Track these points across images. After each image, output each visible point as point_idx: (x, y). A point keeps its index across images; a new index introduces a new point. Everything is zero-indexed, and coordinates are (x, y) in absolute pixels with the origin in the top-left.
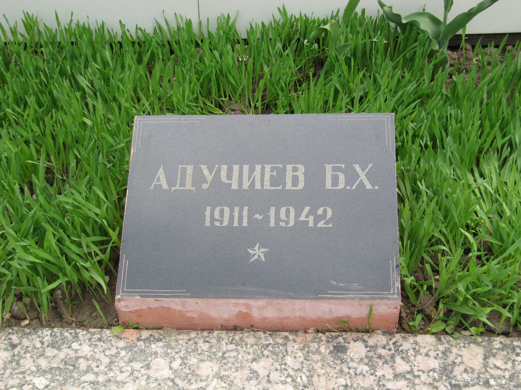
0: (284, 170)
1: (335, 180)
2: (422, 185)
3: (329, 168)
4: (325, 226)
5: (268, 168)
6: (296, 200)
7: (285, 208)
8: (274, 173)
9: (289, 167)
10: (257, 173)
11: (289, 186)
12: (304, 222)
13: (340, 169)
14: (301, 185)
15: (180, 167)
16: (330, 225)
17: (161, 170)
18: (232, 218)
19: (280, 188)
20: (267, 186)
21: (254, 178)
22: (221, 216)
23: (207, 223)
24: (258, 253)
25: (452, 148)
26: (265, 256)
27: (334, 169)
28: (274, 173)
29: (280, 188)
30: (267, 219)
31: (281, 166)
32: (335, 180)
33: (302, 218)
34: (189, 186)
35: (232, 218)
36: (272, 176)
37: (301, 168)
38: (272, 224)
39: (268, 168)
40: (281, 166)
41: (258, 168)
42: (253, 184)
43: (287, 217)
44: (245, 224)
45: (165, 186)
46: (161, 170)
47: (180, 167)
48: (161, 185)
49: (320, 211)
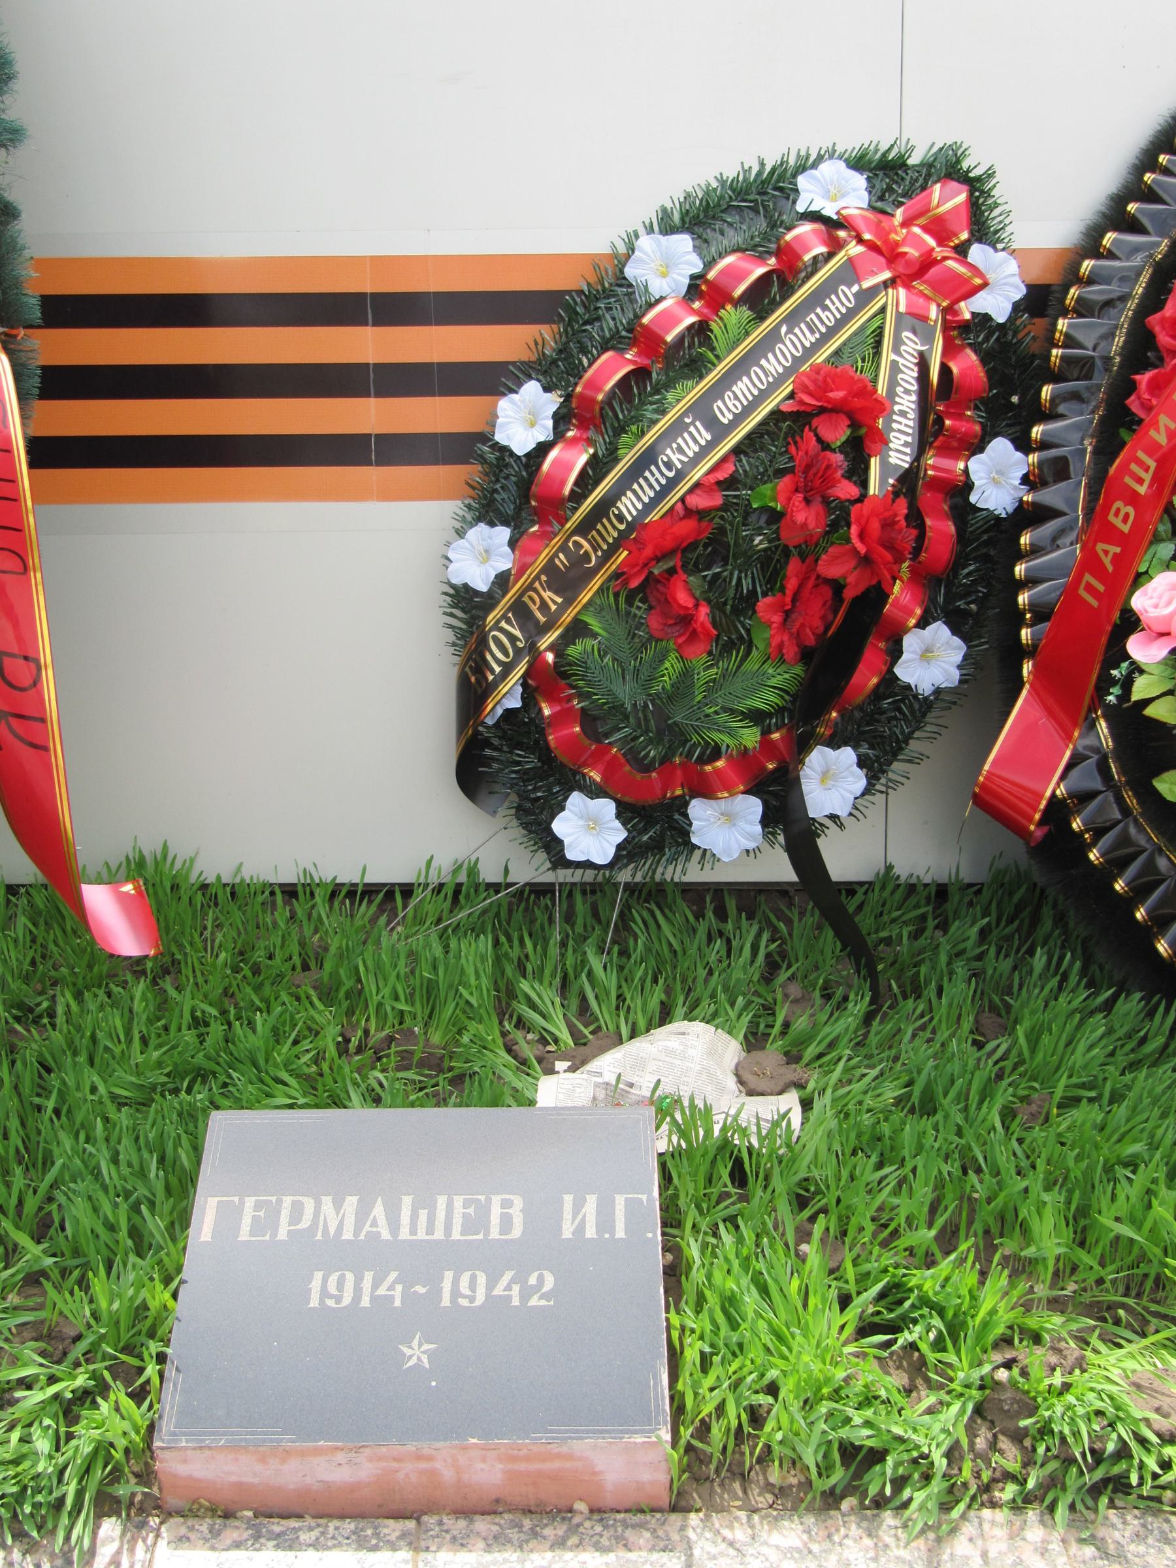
4: (543, 1303)
5: (458, 1201)
6: (492, 1258)
7: (536, 1274)
8: (262, 1214)
9: (496, 1200)
11: (495, 1234)
14: (517, 1232)
17: (379, 1202)
18: (358, 1290)
19: (480, 1236)
20: (456, 1235)
21: (325, 1222)
22: (331, 1289)
23: (314, 1303)
24: (417, 1353)
28: (471, 1210)
29: (480, 1236)
31: (482, 1198)
33: (498, 1291)
34: (495, 1234)
35: (358, 1290)
36: (255, 1219)
37: (518, 1202)
38: (446, 1301)
39: (458, 1201)
40: (482, 1198)
42: (580, 1229)
43: (470, 1289)
44: (365, 1302)
45: (386, 1235)
46: (379, 1202)
48: (379, 1233)
49: (533, 1280)
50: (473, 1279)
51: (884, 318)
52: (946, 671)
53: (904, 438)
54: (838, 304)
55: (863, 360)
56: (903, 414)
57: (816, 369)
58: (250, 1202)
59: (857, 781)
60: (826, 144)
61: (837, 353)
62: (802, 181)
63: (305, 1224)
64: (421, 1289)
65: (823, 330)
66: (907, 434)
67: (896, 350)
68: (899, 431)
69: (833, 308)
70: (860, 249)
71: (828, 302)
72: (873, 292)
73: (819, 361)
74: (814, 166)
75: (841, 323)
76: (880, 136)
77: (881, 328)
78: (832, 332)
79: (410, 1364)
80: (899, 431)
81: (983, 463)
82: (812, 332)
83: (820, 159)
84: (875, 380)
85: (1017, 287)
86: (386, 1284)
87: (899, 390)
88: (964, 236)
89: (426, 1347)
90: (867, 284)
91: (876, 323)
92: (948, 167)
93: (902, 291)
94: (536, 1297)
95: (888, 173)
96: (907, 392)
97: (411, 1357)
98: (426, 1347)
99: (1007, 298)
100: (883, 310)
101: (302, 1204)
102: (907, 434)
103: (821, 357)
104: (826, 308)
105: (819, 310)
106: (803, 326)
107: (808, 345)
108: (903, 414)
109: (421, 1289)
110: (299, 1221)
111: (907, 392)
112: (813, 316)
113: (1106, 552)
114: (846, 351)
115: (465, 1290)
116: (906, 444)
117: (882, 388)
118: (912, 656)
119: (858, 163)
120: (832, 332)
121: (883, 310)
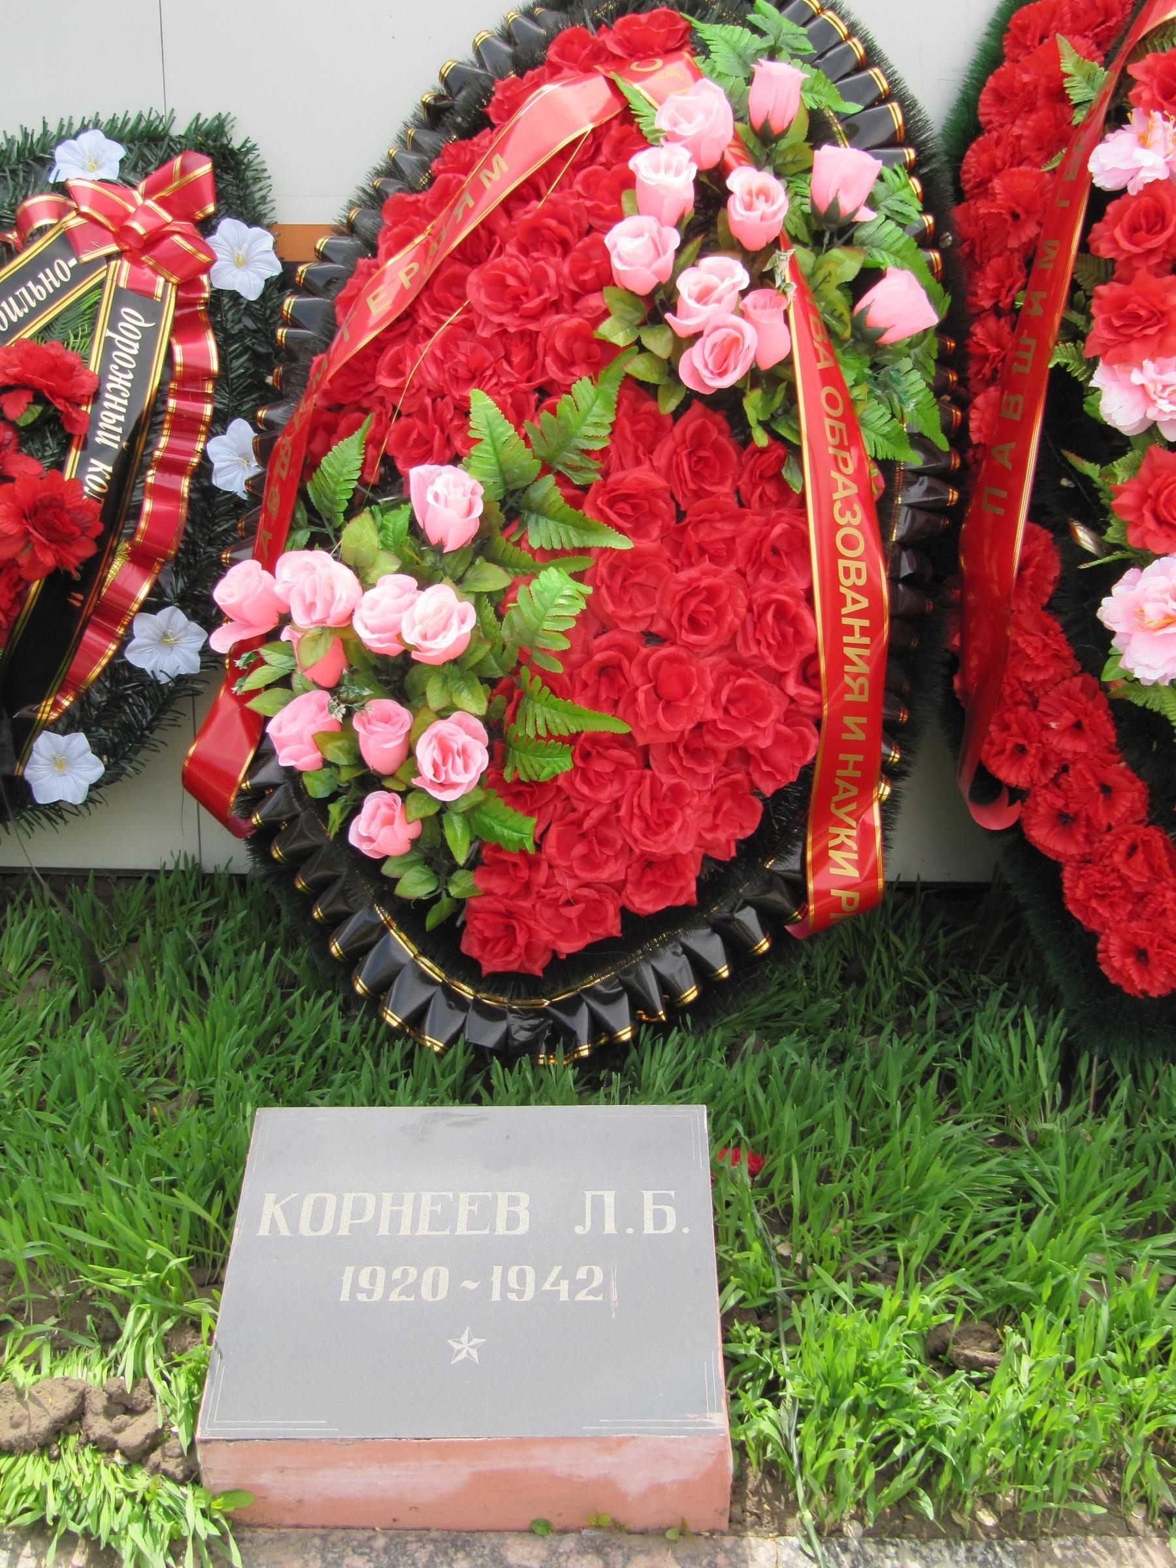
0: (495, 1198)
1: (660, 1219)
2: (273, 1222)
3: (648, 1196)
4: (591, 1298)
8: (438, 1208)
9: (503, 1198)
10: (407, 1210)
11: (501, 1229)
12: (548, 1292)
13: (666, 1200)
14: (523, 1229)
15: (589, 1194)
16: (600, 1298)
20: (423, 1230)
22: (365, 1284)
23: (345, 1297)
24: (466, 1347)
25: (902, 1164)
26: (451, 1349)
27: (657, 1200)
30: (487, 1287)
31: (489, 1194)
32: (660, 1219)
33: (547, 1286)
36: (433, 1214)
37: (525, 1199)
38: (496, 1296)
39: (426, 1198)
41: (409, 1197)
43: (515, 1284)
47: (589, 1194)
50: (373, 1275)
51: (102, 294)
52: (186, 658)
53: (115, 417)
54: (50, 279)
55: (76, 337)
56: (116, 392)
57: (20, 342)
58: (464, 1197)
59: (93, 768)
60: (90, 116)
61: (47, 328)
62: (61, 153)
63: (368, 1218)
64: (471, 1285)
65: (33, 304)
66: (119, 413)
67: (113, 326)
68: (112, 410)
69: (46, 282)
70: (80, 221)
71: (41, 276)
72: (94, 264)
73: (26, 336)
74: (75, 137)
75: (52, 298)
76: (135, 103)
77: (98, 303)
78: (42, 306)
79: (459, 1358)
80: (112, 410)
81: (225, 444)
82: (21, 306)
83: (84, 128)
84: (87, 358)
85: (271, 264)
86: (551, 1279)
87: (113, 367)
88: (211, 208)
89: (475, 1341)
90: (86, 258)
91: (93, 298)
92: (212, 140)
93: (126, 264)
94: (585, 1291)
95: (145, 144)
96: (122, 370)
97: (459, 1351)
98: (475, 1341)
99: (260, 275)
100: (101, 285)
101: (365, 1200)
102: (119, 413)
103: (27, 333)
104: (38, 282)
105: (30, 284)
106: (11, 300)
107: (14, 319)
108: (116, 392)
109: (471, 1285)
110: (360, 1217)
111: (122, 370)
112: (23, 290)
113: (855, 601)
114: (58, 327)
115: (513, 1284)
116: (118, 424)
117: (94, 366)
118: (146, 641)
119: (114, 132)
120: (42, 306)
121: (101, 285)
